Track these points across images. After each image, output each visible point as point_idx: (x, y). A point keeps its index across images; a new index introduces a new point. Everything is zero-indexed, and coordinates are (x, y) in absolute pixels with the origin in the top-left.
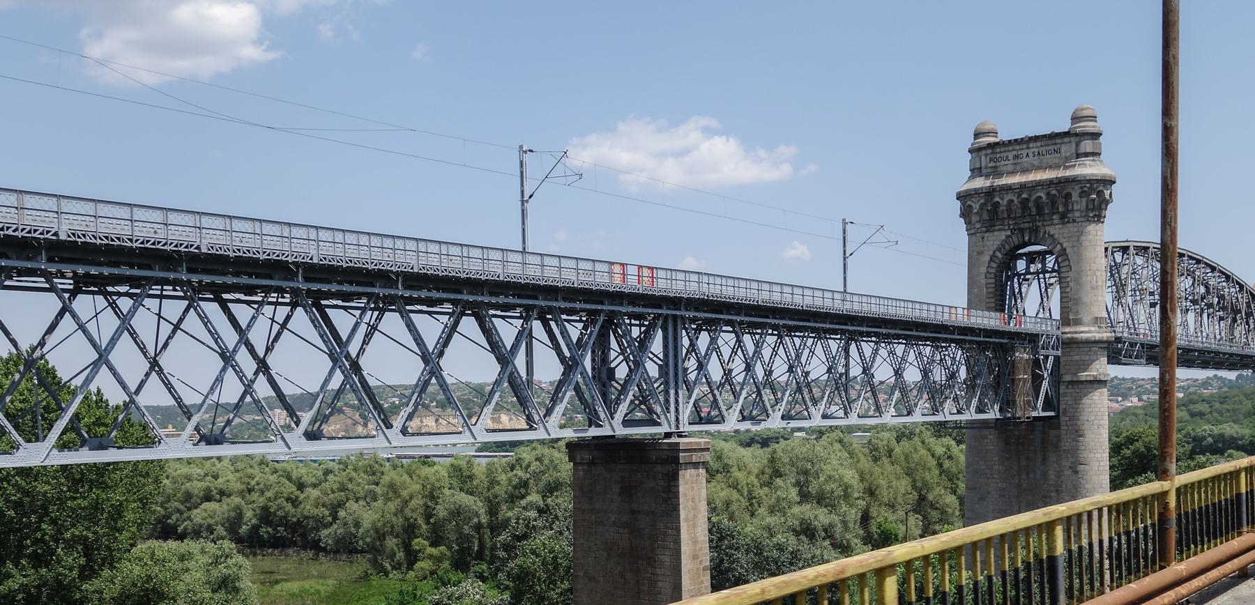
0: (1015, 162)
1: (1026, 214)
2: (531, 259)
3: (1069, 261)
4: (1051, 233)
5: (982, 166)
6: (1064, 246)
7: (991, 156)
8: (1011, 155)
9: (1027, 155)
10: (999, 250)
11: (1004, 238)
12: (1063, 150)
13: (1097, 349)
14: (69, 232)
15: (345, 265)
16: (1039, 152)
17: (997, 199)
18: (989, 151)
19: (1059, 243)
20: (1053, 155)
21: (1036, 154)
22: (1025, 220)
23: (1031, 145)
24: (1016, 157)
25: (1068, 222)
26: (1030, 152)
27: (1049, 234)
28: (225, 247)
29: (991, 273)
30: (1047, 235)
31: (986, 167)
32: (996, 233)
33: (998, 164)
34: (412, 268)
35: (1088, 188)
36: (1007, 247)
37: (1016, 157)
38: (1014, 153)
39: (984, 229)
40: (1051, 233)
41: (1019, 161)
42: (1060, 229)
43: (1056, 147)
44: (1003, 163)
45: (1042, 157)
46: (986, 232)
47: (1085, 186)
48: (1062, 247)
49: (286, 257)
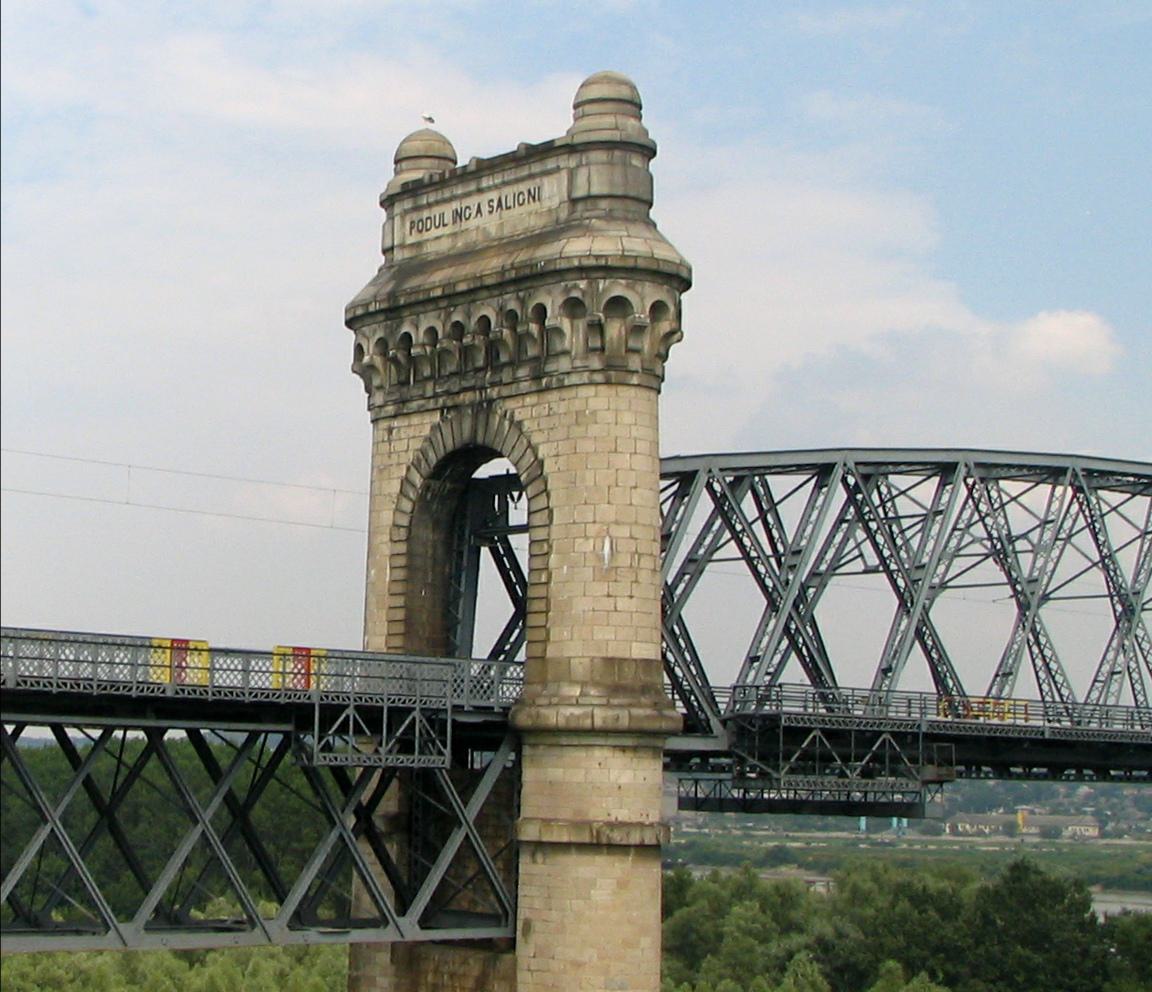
0: (457, 228)
1: (468, 369)
2: (193, 660)
3: (548, 496)
4: (517, 417)
5: (396, 243)
6: (542, 453)
7: (415, 216)
8: (448, 210)
9: (479, 211)
10: (416, 464)
11: (426, 431)
12: (545, 193)
13: (607, 753)
14: (20, 680)
15: (55, 690)
16: (500, 201)
17: (406, 328)
18: (408, 204)
19: (529, 445)
20: (527, 208)
21: (495, 204)
22: (465, 384)
23: (485, 183)
24: (458, 215)
25: (548, 389)
26: (484, 199)
27: (512, 422)
28: (377, 697)
29: (400, 527)
30: (507, 423)
31: (402, 246)
32: (415, 420)
33: (426, 235)
34: (163, 692)
35: (584, 293)
36: (431, 455)
37: (458, 215)
38: (455, 205)
39: (390, 409)
40: (517, 417)
41: (465, 225)
42: (533, 406)
43: (530, 185)
44: (434, 233)
45: (506, 213)
46: (395, 416)
47: (576, 287)
48: (536, 458)
49: (277, 698)
